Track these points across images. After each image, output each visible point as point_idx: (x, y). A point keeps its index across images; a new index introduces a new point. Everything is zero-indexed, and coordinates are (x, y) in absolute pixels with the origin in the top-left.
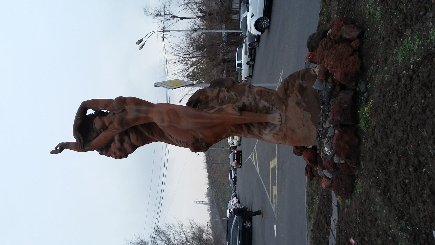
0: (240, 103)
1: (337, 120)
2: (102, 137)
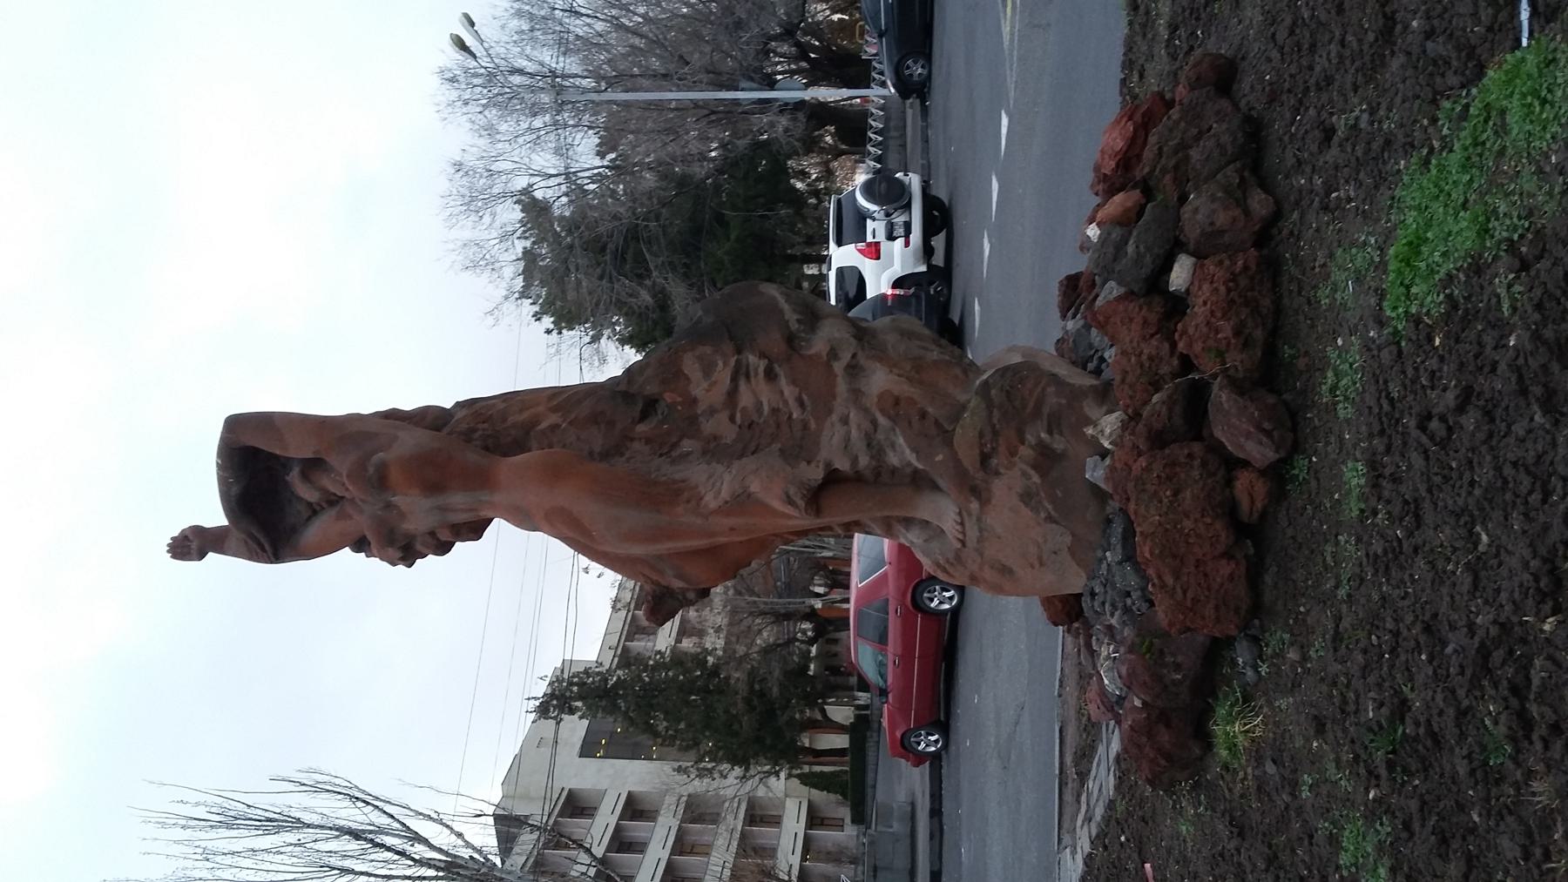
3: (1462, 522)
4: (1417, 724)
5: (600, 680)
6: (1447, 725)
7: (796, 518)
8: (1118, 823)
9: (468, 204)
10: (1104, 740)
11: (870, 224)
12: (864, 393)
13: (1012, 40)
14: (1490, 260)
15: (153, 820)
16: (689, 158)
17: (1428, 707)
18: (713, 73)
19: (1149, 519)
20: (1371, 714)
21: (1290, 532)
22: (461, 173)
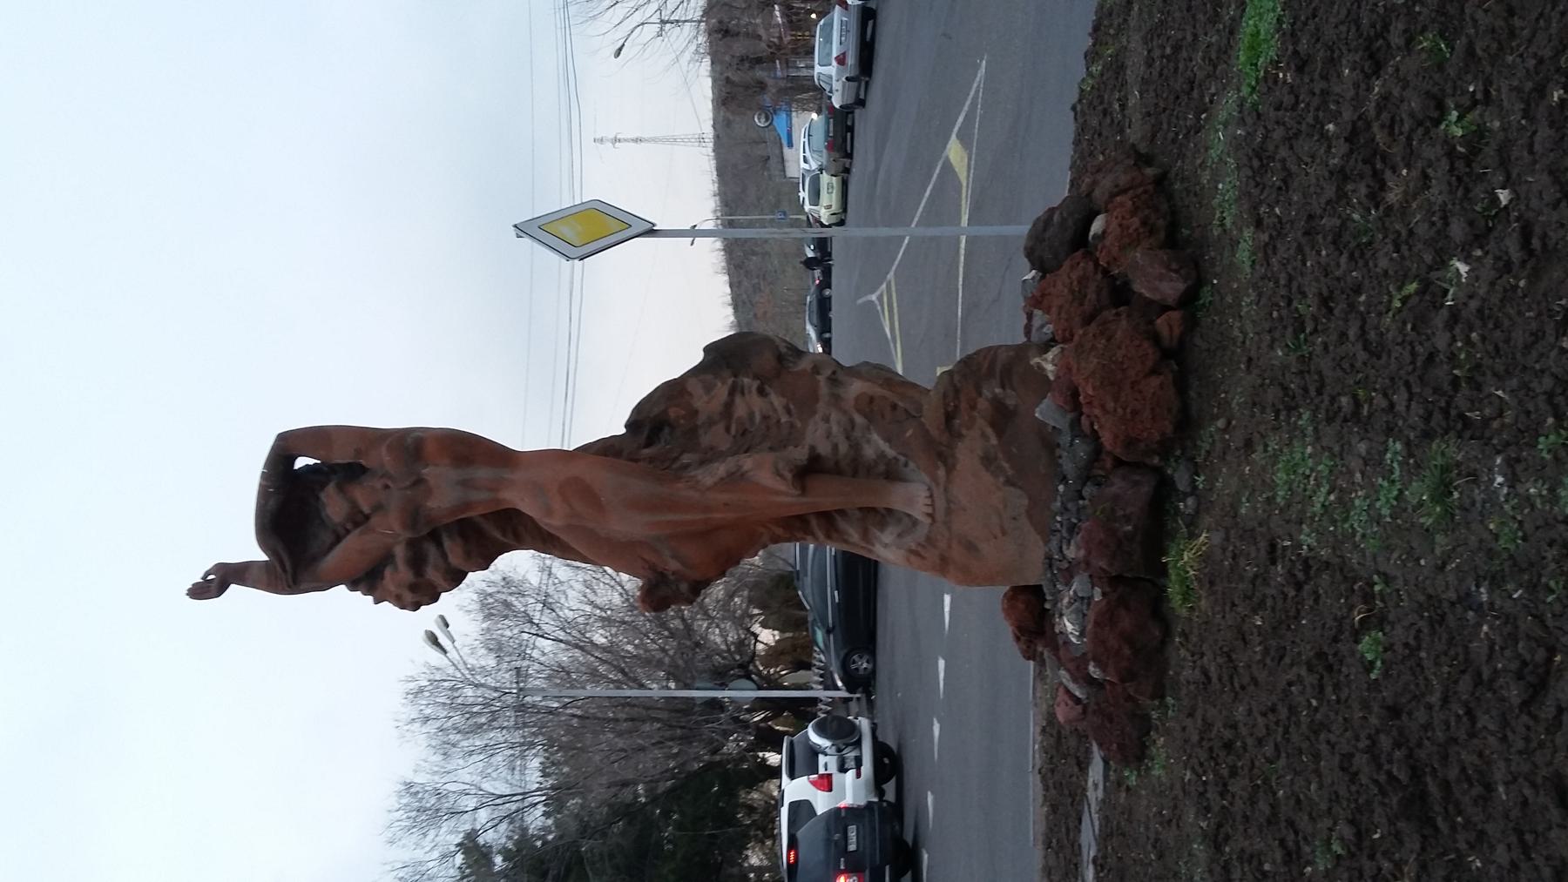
0: (799, 448)
1: (1101, 568)
2: (351, 548)
11: (822, 759)
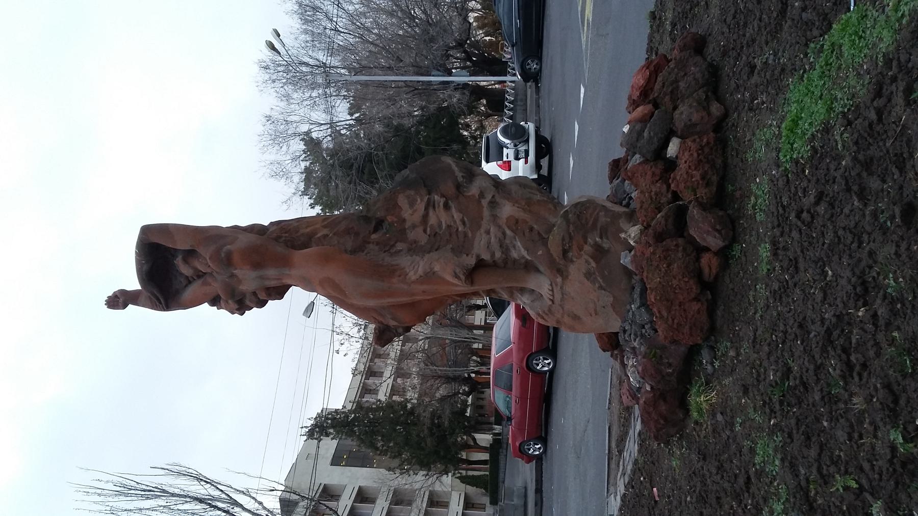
3: (819, 265)
4: (795, 379)
5: (344, 417)
6: (810, 378)
7: (460, 286)
8: (639, 470)
9: (274, 140)
10: (633, 427)
11: (505, 151)
12: (499, 217)
13: (587, 45)
14: (833, 124)
15: (81, 490)
16: (402, 115)
17: (801, 368)
18: (417, 67)
19: (654, 280)
20: (772, 377)
21: (731, 286)
22: (270, 122)
